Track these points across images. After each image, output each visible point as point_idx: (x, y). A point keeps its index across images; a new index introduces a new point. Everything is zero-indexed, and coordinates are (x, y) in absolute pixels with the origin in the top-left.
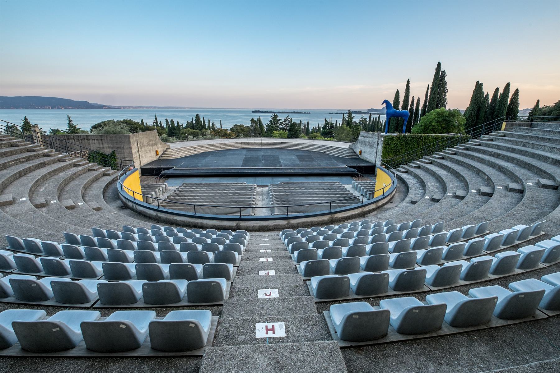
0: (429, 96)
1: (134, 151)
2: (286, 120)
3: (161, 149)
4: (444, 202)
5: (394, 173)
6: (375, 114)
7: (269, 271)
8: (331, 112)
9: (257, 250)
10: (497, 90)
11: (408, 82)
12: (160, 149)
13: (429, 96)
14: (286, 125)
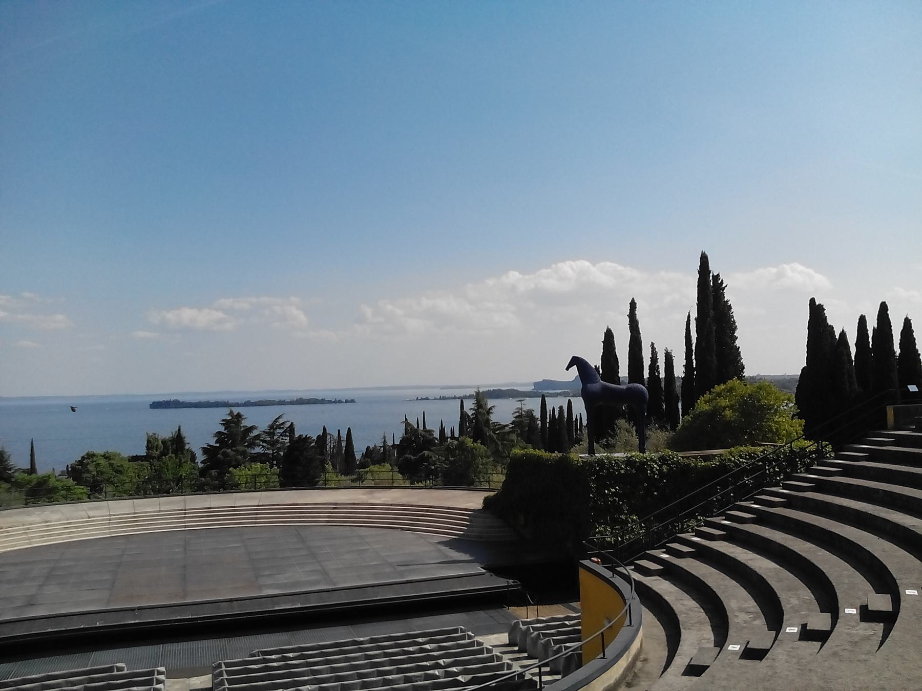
0: (694, 341)
4: (779, 654)
6: (556, 395)
10: (862, 321)
11: (633, 305)
13: (694, 341)
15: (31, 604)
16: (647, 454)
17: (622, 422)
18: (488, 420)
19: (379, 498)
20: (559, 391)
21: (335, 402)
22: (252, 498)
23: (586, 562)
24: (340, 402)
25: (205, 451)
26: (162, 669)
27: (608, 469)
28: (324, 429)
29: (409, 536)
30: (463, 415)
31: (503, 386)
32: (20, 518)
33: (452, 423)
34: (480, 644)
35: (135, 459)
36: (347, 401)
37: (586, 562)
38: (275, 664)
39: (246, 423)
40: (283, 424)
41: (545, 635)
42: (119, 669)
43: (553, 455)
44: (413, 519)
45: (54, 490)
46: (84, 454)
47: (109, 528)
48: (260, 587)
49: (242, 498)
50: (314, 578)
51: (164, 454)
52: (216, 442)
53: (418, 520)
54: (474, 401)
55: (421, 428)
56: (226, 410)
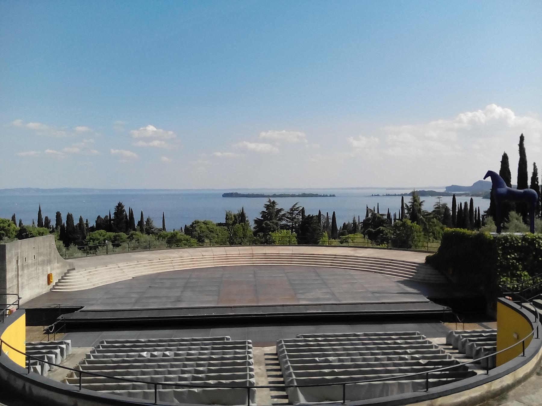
8: (376, 192)
11: (522, 138)
12: (56, 270)
15: (179, 300)
16: (535, 234)
17: (513, 214)
18: (420, 209)
19: (360, 253)
20: (462, 193)
21: (324, 196)
22: (288, 250)
23: (502, 299)
24: (326, 196)
25: (256, 222)
26: (250, 341)
27: (510, 243)
28: (320, 212)
29: (382, 276)
31: (426, 188)
32: (168, 255)
34: (430, 343)
35: (220, 225)
36: (330, 196)
37: (502, 299)
38: (311, 343)
39: (278, 207)
40: (298, 208)
41: (470, 341)
42: (228, 339)
43: (473, 232)
44: (382, 266)
45: (180, 240)
46: (193, 221)
47: (214, 262)
48: (298, 299)
49: (283, 249)
50: (328, 296)
51: (234, 223)
52: (262, 217)
53: (385, 268)
54: (411, 197)
56: (267, 199)
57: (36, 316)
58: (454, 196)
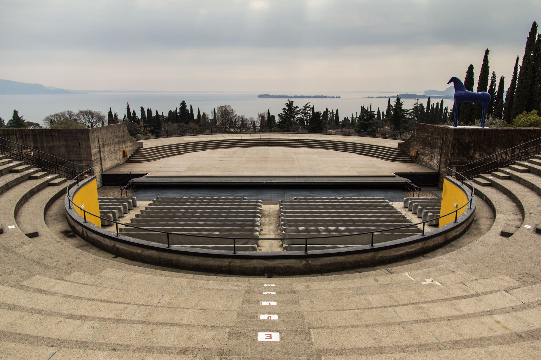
1: (94, 151)
2: (306, 107)
3: (131, 148)
5: (471, 187)
7: (271, 315)
9: (258, 302)
14: (305, 114)
24: (334, 97)
28: (327, 109)
30: (389, 105)
33: (384, 108)
36: (337, 97)
54: (396, 99)
55: (369, 110)
57: (109, 180)
58: (429, 98)
